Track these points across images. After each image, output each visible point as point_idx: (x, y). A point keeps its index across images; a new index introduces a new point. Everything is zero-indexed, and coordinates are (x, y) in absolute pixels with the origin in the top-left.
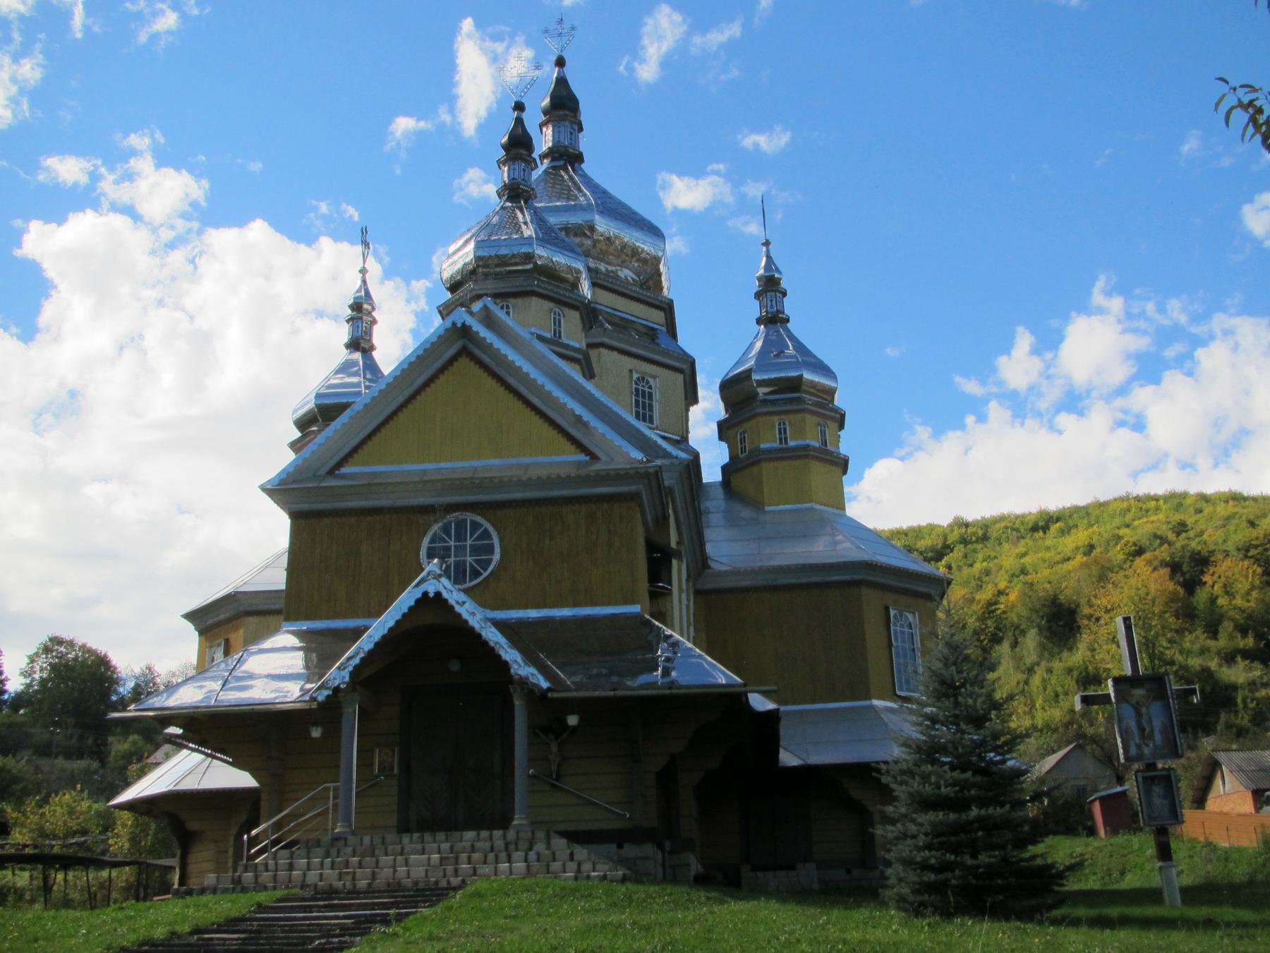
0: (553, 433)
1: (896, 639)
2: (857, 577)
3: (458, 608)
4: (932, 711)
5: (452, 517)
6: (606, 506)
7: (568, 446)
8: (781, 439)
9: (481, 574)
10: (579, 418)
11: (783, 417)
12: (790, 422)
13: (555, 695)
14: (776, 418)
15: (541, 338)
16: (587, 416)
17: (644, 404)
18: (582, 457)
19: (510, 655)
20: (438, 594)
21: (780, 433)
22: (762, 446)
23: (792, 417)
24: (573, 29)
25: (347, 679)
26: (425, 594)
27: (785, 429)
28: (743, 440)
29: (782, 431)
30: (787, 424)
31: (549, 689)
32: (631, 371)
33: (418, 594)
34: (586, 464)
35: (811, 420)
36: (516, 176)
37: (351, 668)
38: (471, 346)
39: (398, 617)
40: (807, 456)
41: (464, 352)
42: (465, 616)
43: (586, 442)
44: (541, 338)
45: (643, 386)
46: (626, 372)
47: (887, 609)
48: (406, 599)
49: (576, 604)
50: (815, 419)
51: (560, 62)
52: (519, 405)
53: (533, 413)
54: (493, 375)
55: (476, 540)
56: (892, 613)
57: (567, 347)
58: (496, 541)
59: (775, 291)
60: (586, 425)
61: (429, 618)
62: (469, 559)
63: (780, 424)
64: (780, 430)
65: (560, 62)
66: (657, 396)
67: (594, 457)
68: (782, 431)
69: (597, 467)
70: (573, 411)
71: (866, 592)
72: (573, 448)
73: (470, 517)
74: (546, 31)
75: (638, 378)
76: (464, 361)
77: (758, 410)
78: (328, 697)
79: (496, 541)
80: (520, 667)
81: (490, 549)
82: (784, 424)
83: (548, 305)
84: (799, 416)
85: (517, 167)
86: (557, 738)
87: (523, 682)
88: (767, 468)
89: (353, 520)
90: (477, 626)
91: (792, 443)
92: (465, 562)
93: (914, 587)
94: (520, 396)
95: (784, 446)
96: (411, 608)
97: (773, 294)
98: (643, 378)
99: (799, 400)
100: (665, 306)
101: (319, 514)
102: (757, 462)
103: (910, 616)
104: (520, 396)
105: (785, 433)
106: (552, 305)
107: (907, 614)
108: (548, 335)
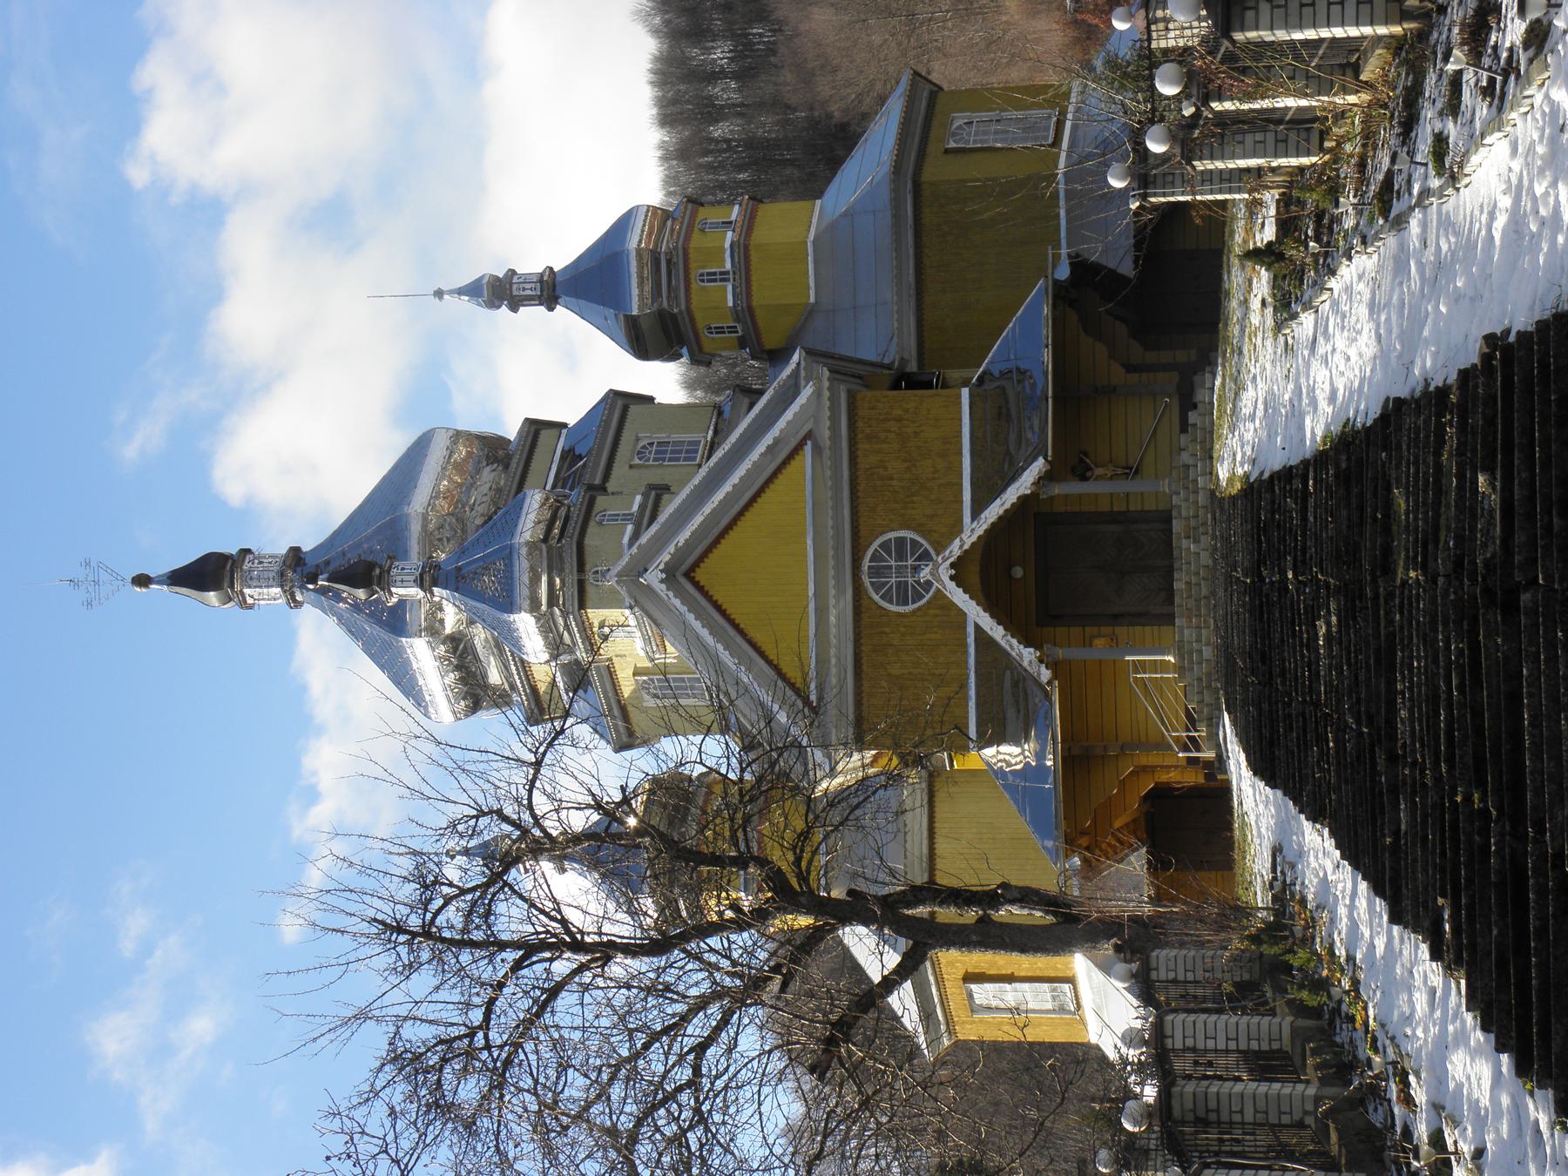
0: (782, 479)
1: (986, 141)
2: (909, 185)
3: (966, 547)
4: (1087, 643)
5: (866, 580)
6: (860, 424)
7: (794, 463)
8: (722, 280)
9: (926, 550)
10: (770, 449)
11: (692, 276)
12: (700, 268)
13: (1050, 453)
14: (694, 286)
15: (636, 536)
16: (768, 440)
17: (680, 452)
18: (808, 448)
19: (1011, 496)
20: (952, 566)
21: (715, 280)
22: (730, 304)
23: (693, 265)
24: (88, 564)
25: (1032, 650)
26: (952, 578)
27: (708, 274)
28: (720, 330)
29: (712, 277)
30: (701, 271)
31: (1045, 459)
32: (631, 467)
33: (951, 585)
34: (817, 450)
35: (697, 240)
36: (413, 578)
37: (1022, 647)
38: (684, 567)
39: (973, 603)
40: (746, 247)
41: (689, 575)
42: (974, 538)
43: (793, 443)
44: (636, 536)
45: (650, 453)
46: (634, 472)
47: (947, 151)
48: (959, 597)
49: (960, 454)
50: (696, 235)
51: (142, 581)
52: (733, 534)
53: (759, 500)
54: (716, 542)
55: (890, 556)
56: (952, 145)
57: (643, 507)
58: (892, 535)
59: (511, 284)
60: (777, 441)
61: (974, 578)
62: (910, 562)
63: (703, 281)
64: (709, 281)
65: (142, 581)
66: (662, 436)
67: (809, 435)
68: (712, 277)
69: (825, 434)
70: (762, 455)
71: (928, 175)
72: (798, 458)
73: (866, 563)
74: (89, 604)
75: (640, 459)
76: (699, 575)
77: (683, 307)
78: (1047, 668)
79: (892, 535)
80: (1024, 484)
81: (901, 542)
82: (702, 275)
83: (592, 529)
84: (692, 256)
85: (399, 578)
86: (1091, 469)
87: (1041, 481)
88: (757, 301)
89: (866, 684)
90: (985, 527)
91: (728, 266)
92: (907, 582)
93: (920, 119)
94: (741, 514)
95: (731, 276)
96: (965, 592)
97: (515, 287)
98: (639, 453)
99: (669, 254)
100: (532, 430)
101: (859, 722)
102: (750, 310)
103: (956, 124)
104: (741, 514)
105: (715, 274)
106: (592, 524)
107: (955, 126)
108: (630, 528)
